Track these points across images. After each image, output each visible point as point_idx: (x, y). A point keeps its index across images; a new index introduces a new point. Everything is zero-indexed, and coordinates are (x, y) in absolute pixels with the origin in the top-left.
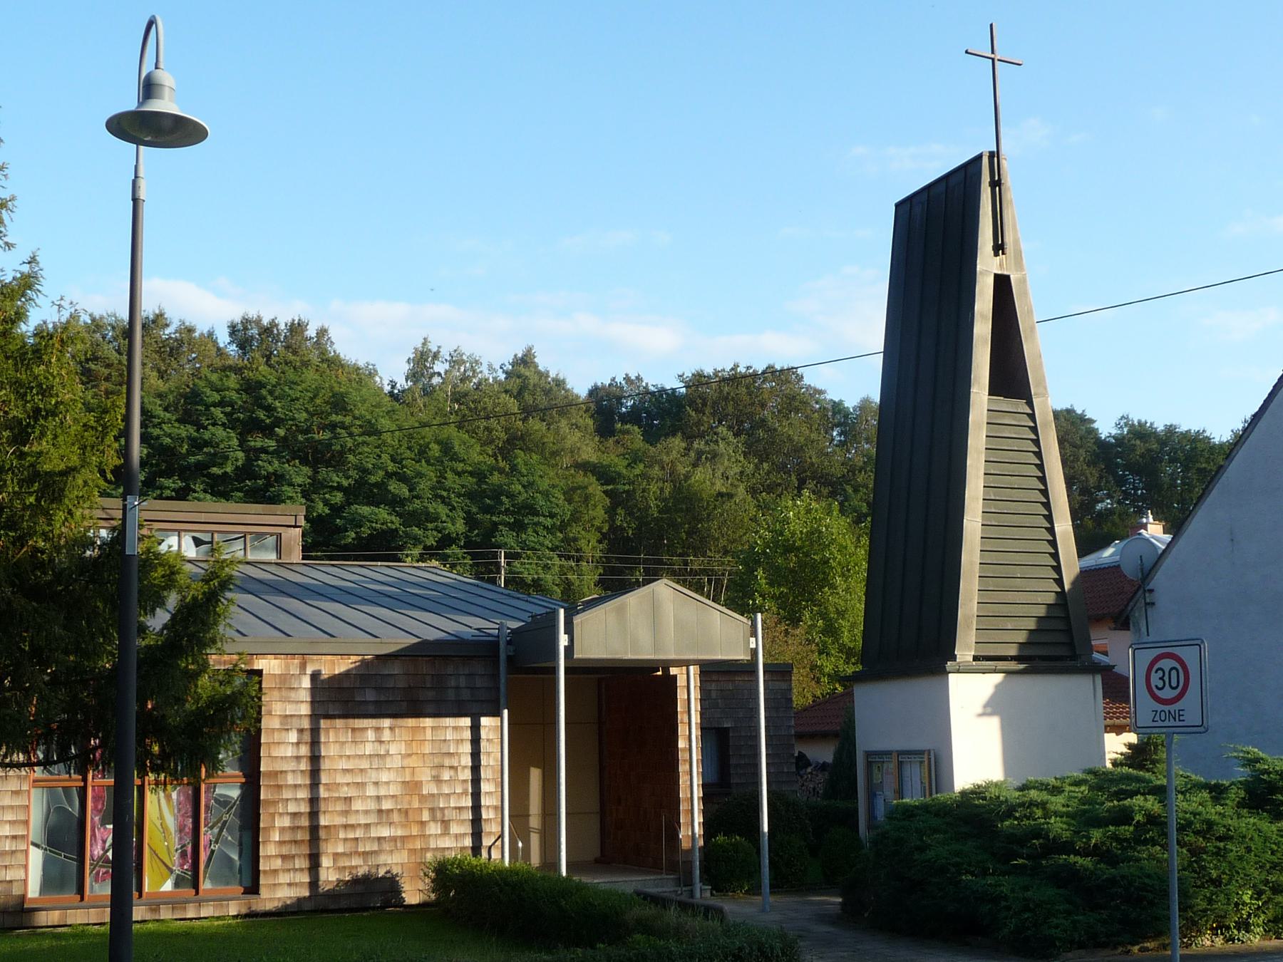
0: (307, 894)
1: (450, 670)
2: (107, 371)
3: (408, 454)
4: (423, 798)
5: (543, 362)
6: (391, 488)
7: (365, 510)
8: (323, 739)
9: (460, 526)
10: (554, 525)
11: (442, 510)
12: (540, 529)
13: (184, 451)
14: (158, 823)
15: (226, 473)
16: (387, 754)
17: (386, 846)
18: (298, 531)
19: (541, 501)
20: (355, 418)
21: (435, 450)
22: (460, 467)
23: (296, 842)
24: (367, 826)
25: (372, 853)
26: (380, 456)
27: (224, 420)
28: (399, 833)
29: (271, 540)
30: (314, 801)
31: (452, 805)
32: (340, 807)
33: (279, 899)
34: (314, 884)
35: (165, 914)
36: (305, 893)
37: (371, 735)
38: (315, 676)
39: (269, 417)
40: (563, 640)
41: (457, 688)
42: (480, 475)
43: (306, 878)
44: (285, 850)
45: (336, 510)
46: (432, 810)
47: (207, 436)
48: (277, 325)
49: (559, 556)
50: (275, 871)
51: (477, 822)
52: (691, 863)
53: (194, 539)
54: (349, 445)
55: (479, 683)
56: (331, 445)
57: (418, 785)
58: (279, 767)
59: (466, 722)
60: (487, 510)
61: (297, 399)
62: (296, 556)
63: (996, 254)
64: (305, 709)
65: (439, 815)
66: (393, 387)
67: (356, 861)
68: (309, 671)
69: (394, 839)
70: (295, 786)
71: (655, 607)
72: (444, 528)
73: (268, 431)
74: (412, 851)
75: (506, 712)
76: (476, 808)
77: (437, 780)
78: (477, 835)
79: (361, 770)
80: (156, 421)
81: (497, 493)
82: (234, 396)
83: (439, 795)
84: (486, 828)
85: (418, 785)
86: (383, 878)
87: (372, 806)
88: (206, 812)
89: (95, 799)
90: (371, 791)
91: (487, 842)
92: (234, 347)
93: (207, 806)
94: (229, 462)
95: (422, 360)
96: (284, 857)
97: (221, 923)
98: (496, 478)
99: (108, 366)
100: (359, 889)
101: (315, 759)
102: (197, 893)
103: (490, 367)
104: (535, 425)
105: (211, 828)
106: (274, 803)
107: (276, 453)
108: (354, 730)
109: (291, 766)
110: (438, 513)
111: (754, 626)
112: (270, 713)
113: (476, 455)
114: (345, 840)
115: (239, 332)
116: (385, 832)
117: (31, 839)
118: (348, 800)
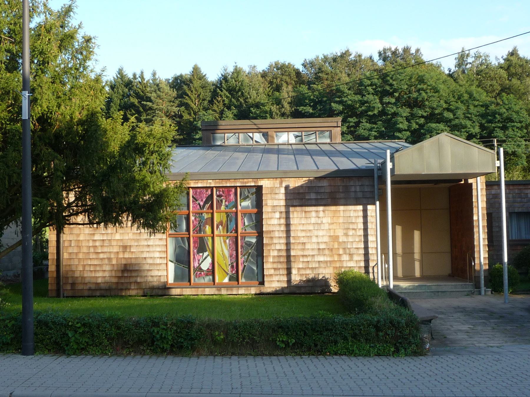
0: (286, 286)
1: (352, 183)
2: (326, 76)
3: (453, 99)
4: (339, 243)
5: (522, 53)
6: (445, 115)
8: (291, 216)
9: (477, 130)
10: (522, 126)
11: (468, 123)
12: (515, 129)
13: (358, 106)
14: (221, 253)
15: (374, 114)
16: (322, 223)
17: (322, 265)
18: (339, 129)
19: (515, 116)
20: (428, 86)
21: (466, 96)
23: (280, 262)
24: (313, 256)
25: (316, 268)
26: (439, 101)
27: (373, 91)
28: (329, 259)
29: (327, 134)
30: (288, 244)
31: (354, 247)
32: (300, 247)
33: (273, 287)
34: (289, 281)
35: (224, 292)
36: (285, 285)
37: (314, 214)
38: (287, 188)
39: (391, 89)
40: (389, 165)
41: (355, 192)
42: (486, 106)
43: (285, 279)
44: (275, 266)
45: (421, 126)
46: (344, 249)
47: (365, 99)
48: (398, 50)
50: (271, 275)
51: (366, 254)
52: (479, 277)
54: (426, 98)
55: (366, 189)
56: (418, 98)
57: (337, 237)
58: (271, 228)
59: (360, 207)
60: (490, 122)
61: (403, 80)
62: (339, 139)
64: (283, 203)
65: (348, 251)
67: (308, 272)
68: (284, 185)
69: (326, 262)
70: (279, 237)
71: (440, 147)
72: (470, 131)
73: (391, 94)
74: (335, 268)
75: (378, 203)
76: (366, 248)
77: (346, 235)
78: (367, 261)
79: (310, 230)
80: (345, 94)
81: (494, 114)
82: (376, 81)
83: (348, 242)
84: (371, 257)
85: (337, 237)
86: (321, 279)
87: (316, 247)
88: (241, 249)
89: (194, 242)
90: (314, 240)
91: (372, 264)
92: (381, 61)
93: (242, 246)
94: (376, 110)
95: (462, 58)
96: (275, 269)
97: (246, 297)
98: (493, 107)
99: (327, 74)
100: (310, 284)
101: (288, 225)
102: (238, 284)
103: (497, 58)
104: (515, 81)
105: (244, 256)
106: (270, 245)
107: (395, 104)
108: (305, 212)
109: (277, 228)
110: (466, 125)
111: (498, 154)
112: (266, 205)
113: (484, 97)
114: (303, 262)
115: (383, 55)
116: (322, 259)
117: (169, 258)
118: (304, 244)
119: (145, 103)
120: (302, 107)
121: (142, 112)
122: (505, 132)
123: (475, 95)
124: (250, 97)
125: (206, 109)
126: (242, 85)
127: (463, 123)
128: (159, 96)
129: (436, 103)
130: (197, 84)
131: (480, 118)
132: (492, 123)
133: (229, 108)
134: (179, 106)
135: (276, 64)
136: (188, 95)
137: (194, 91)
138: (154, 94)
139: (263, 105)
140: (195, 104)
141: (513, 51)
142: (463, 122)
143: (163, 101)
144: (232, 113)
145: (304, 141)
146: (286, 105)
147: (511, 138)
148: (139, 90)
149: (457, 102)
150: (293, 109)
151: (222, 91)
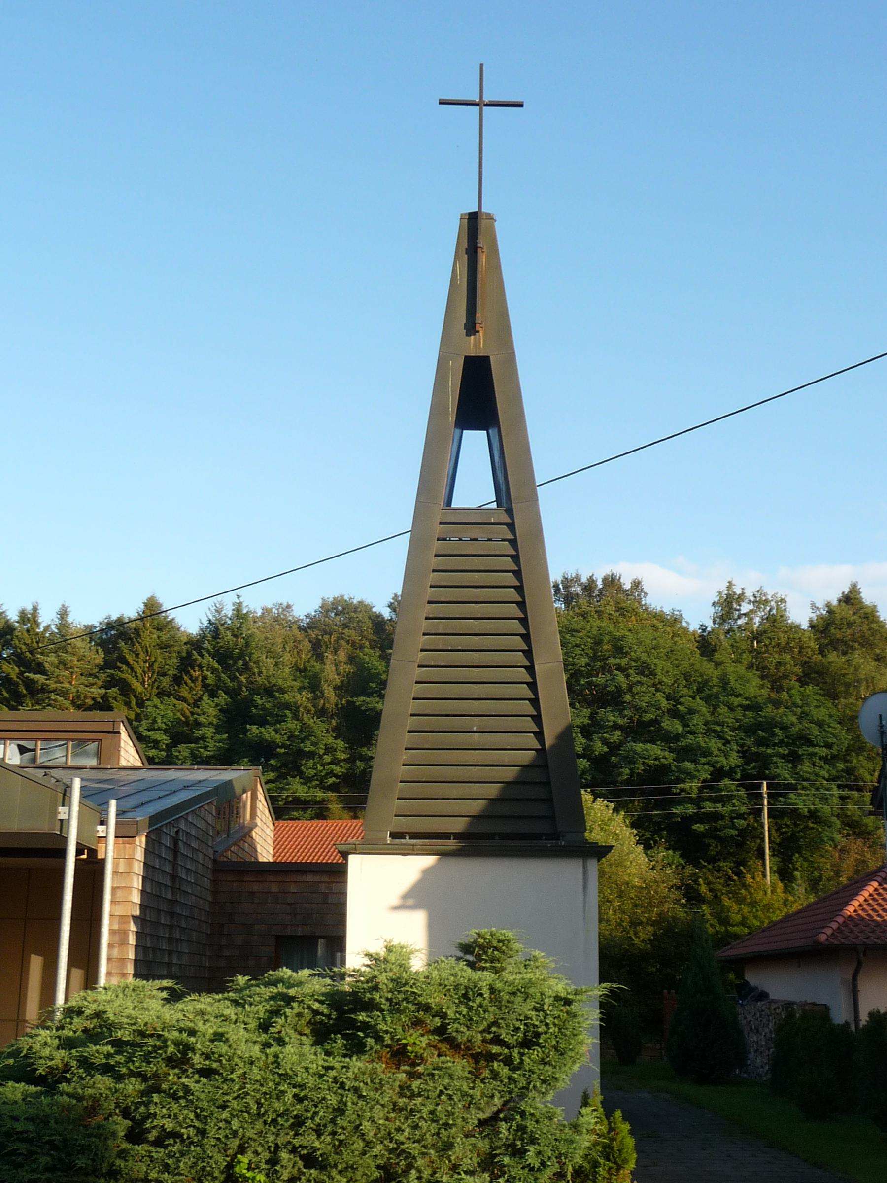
3: (685, 691)
5: (868, 597)
7: (639, 747)
9: (734, 759)
11: (714, 744)
22: (736, 701)
29: (93, 746)
42: (754, 707)
45: (614, 748)
49: (839, 787)
53: (19, 746)
60: (761, 743)
63: (468, 334)
66: (704, 631)
72: (717, 762)
95: (728, 604)
98: (769, 711)
104: (833, 657)
119: (31, 675)
120: (362, 698)
121: (25, 696)
122: (795, 767)
123: (732, 683)
124: (260, 673)
125: (162, 694)
126: (247, 645)
127: (703, 745)
128: (63, 663)
129: (648, 699)
130: (150, 638)
131: (742, 735)
132: (768, 746)
133: (213, 695)
134: (107, 686)
135: (336, 602)
136: (128, 664)
137: (142, 655)
138: (52, 658)
139: (282, 691)
140: (143, 683)
141: (850, 592)
142: (701, 740)
143: (72, 673)
144: (217, 705)
145: (39, 760)
146: (329, 692)
147: (807, 780)
148: (23, 647)
149: (694, 698)
150: (344, 702)
151: (202, 656)
